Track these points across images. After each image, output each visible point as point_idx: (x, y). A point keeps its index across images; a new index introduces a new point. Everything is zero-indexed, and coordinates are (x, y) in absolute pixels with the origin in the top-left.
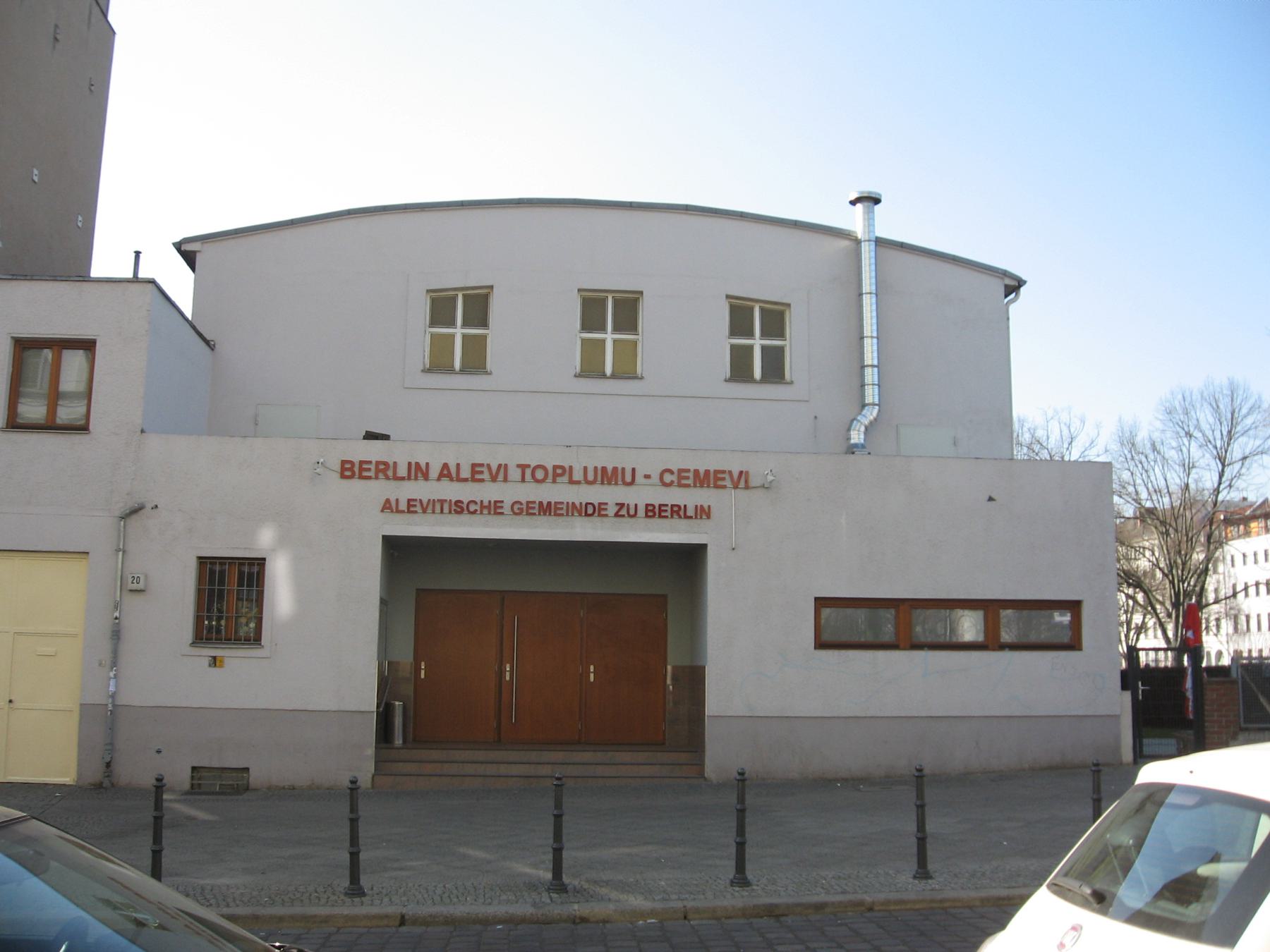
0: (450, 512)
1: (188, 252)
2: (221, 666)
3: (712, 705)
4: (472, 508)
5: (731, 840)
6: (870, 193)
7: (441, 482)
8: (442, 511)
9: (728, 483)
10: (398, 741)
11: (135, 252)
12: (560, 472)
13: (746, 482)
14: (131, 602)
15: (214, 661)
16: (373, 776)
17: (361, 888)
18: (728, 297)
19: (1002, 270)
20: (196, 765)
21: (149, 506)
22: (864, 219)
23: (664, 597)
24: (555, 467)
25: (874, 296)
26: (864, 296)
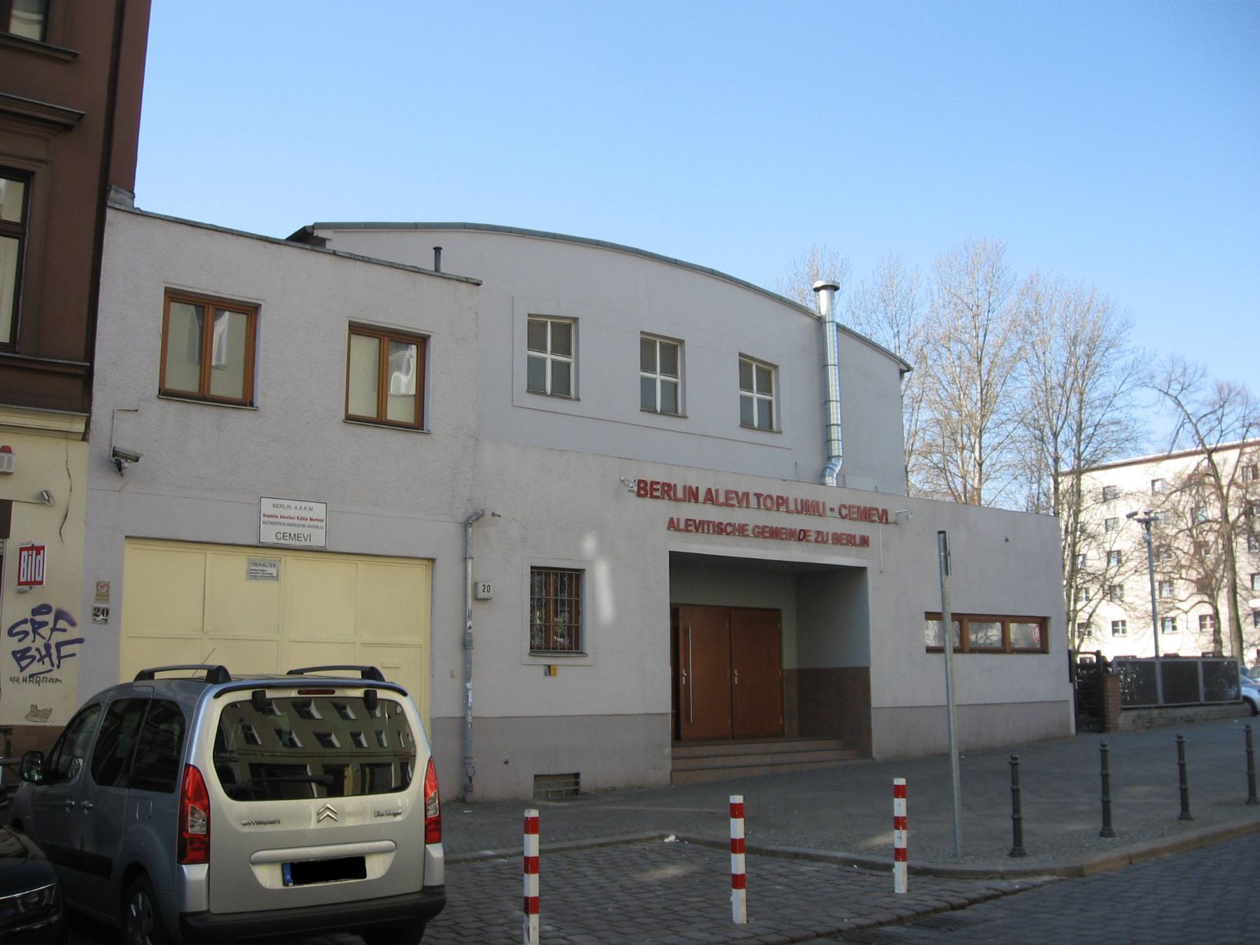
0: (714, 533)
2: (555, 675)
3: (876, 700)
7: (706, 505)
8: (709, 532)
9: (876, 518)
11: (434, 248)
12: (781, 502)
13: (887, 519)
14: (479, 611)
15: (549, 670)
16: (671, 774)
18: (741, 355)
21: (488, 513)
23: (777, 612)
26: (829, 367)
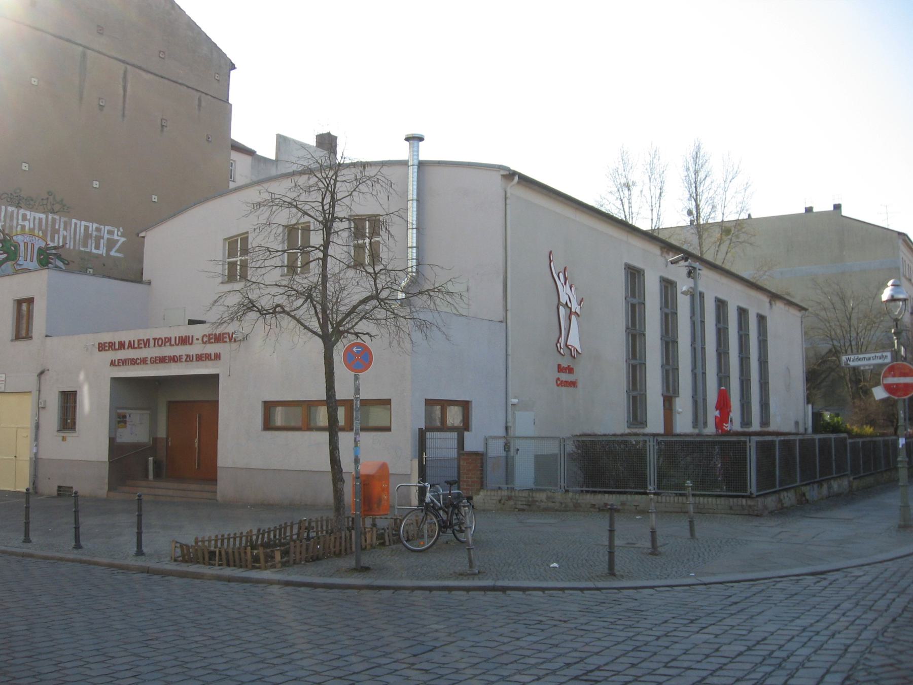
1: (144, 237)
4: (138, 361)
5: (23, 520)
6: (412, 135)
10: (151, 477)
17: (80, 545)
19: (498, 165)
20: (61, 485)
22: (410, 152)
24: (165, 338)
25: (415, 202)
